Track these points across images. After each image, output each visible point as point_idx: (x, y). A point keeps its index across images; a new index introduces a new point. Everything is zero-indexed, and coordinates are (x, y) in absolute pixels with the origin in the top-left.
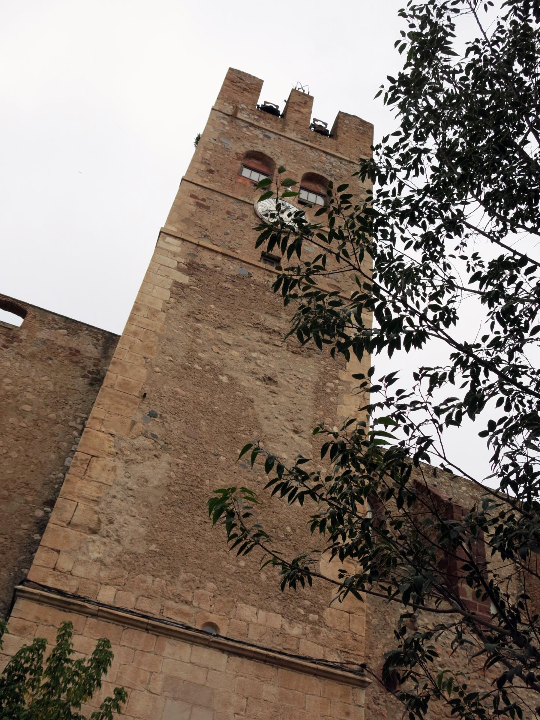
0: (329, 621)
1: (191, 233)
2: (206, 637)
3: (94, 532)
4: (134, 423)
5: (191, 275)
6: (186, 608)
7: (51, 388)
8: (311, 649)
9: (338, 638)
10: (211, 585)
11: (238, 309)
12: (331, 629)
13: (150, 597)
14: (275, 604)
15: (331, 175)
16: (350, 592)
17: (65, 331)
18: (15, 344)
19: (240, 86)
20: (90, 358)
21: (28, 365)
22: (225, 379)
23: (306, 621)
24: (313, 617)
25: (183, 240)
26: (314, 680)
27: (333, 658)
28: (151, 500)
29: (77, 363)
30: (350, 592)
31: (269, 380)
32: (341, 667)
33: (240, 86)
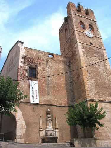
5: (84, 49)
10: (103, 95)
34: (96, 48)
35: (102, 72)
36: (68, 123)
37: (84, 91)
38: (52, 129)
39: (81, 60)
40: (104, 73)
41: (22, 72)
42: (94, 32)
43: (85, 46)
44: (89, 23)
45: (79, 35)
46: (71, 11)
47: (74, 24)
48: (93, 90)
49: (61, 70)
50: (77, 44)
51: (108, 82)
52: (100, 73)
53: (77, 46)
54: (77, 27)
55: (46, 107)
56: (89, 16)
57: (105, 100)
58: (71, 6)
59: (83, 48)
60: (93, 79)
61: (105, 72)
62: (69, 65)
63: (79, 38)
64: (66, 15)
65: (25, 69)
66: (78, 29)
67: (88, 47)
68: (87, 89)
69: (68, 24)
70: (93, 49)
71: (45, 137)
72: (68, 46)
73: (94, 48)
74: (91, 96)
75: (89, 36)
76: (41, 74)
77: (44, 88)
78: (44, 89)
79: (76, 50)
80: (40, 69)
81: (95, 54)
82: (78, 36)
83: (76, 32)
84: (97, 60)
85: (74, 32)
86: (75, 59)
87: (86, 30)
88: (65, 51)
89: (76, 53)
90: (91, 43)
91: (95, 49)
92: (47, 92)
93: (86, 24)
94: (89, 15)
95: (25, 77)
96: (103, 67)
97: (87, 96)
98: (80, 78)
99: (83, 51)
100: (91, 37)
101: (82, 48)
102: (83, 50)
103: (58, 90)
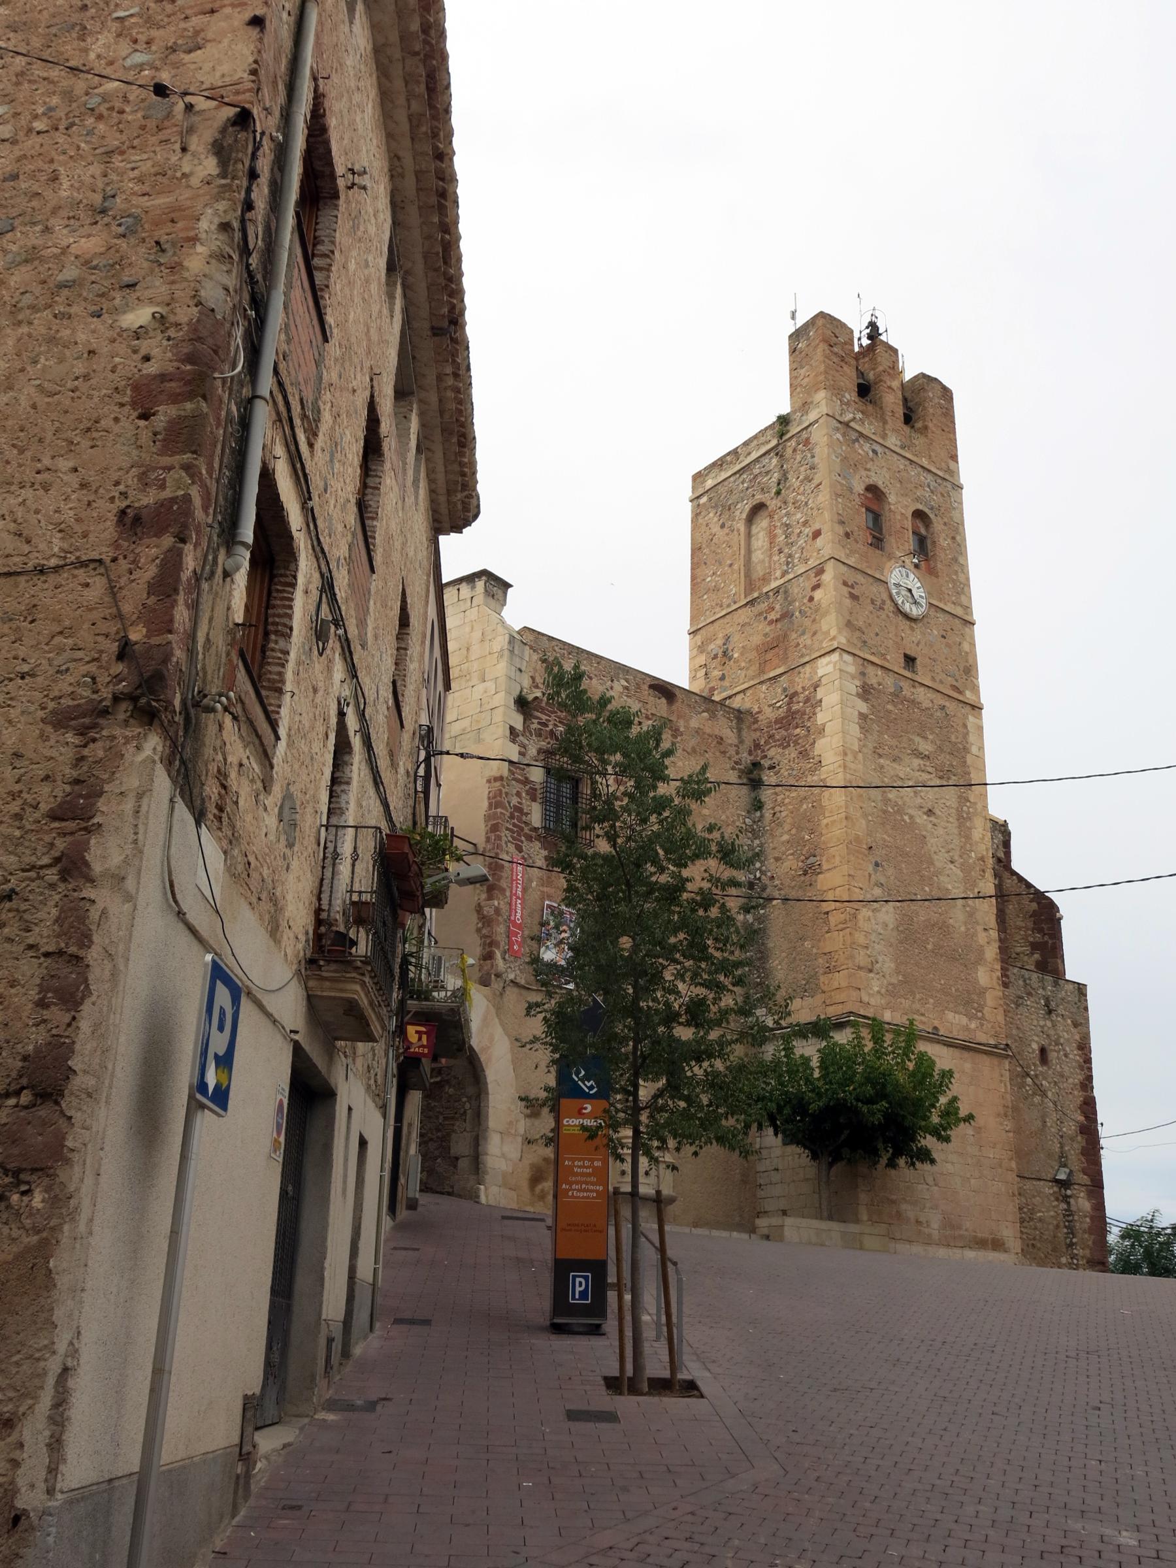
0: (987, 1016)
3: (871, 971)
4: (870, 875)
5: (866, 700)
6: (923, 1018)
8: (982, 1037)
10: (931, 1001)
11: (9, 706)
14: (961, 1008)
17: (705, 714)
19: (511, 586)
20: (731, 745)
22: (906, 818)
24: (979, 1014)
25: (854, 655)
26: (985, 1057)
27: (992, 1042)
28: (892, 940)
31: (930, 812)
32: (995, 1047)
33: (511, 586)
34: (931, 695)
35: (940, 860)
36: (55, 1285)
40: (952, 862)
41: (515, 801)
42: (932, 572)
43: (873, 681)
45: (854, 597)
48: (887, 964)
51: (965, 923)
52: (931, 862)
56: (920, 441)
57: (935, 1028)
61: (956, 858)
64: (785, 409)
65: (526, 781)
66: (852, 552)
67: (889, 682)
70: (914, 703)
71: (54, 1366)
72: (757, 639)
73: (922, 695)
74: (873, 1001)
79: (820, 693)
81: (917, 739)
86: (804, 754)
87: (890, 557)
90: (910, 660)
93: (899, 506)
96: (953, 828)
99: (860, 714)
102: (863, 707)
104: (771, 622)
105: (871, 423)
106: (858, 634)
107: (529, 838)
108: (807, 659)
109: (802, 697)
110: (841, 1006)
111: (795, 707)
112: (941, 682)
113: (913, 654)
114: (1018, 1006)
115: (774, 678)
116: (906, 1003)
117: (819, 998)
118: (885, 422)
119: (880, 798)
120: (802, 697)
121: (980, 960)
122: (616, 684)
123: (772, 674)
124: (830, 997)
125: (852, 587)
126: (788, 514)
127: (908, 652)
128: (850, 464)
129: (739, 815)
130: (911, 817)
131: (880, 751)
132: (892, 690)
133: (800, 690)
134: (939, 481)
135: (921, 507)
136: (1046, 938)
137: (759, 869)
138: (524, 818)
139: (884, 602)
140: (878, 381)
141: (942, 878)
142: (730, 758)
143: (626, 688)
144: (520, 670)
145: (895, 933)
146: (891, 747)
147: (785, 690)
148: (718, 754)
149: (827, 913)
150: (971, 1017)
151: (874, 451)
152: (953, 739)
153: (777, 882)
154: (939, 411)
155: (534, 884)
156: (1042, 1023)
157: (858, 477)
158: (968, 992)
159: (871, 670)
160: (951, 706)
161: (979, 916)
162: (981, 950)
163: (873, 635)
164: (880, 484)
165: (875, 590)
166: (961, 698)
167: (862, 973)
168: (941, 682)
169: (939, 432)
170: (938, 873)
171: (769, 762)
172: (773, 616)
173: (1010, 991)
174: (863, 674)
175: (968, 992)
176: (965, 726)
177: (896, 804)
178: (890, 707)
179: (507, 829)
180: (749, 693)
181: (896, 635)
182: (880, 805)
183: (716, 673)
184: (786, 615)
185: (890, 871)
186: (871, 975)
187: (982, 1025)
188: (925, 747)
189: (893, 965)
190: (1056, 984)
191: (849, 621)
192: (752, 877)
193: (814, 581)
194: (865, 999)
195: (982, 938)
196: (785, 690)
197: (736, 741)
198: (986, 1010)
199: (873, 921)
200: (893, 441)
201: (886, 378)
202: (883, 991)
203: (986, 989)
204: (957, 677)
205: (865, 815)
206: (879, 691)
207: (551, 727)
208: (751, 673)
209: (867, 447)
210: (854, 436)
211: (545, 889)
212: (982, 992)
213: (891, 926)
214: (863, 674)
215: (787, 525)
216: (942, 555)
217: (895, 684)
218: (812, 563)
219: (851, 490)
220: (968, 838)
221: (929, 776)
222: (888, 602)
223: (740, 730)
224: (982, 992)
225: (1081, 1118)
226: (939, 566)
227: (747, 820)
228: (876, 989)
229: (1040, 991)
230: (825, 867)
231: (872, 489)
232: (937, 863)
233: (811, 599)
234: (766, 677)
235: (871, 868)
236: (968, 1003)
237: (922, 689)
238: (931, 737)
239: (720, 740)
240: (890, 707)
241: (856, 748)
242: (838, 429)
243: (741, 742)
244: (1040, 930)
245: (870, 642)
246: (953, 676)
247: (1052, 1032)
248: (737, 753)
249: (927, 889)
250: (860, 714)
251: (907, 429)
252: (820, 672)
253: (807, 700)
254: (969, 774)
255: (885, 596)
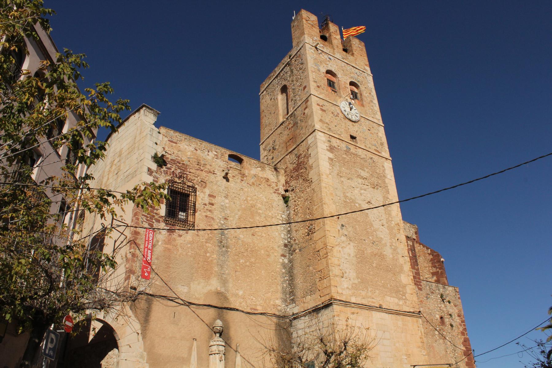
1: (325, 128)
2: (380, 308)
4: (339, 231)
5: (332, 152)
6: (373, 300)
7: (265, 200)
9: (411, 303)
10: (377, 291)
12: (409, 301)
13: (364, 298)
14: (394, 295)
15: (359, 82)
16: (102, 325)
17: (260, 169)
18: (245, 178)
20: (273, 182)
21: (253, 189)
22: (357, 205)
23: (402, 299)
27: (412, 311)
29: (270, 185)
30: (102, 325)
31: (274, 149)
32: (413, 313)
34: (365, 152)
37: (324, 275)
38: (223, 344)
39: (323, 185)
42: (363, 105)
43: (336, 145)
44: (352, 77)
46: (306, 36)
47: (312, 76)
48: (352, 274)
49: (259, 205)
50: (316, 138)
52: (372, 225)
53: (316, 144)
54: (318, 87)
55: (212, 311)
56: (351, 58)
58: (304, 20)
59: (331, 149)
60: (352, 244)
61: (385, 223)
62: (283, 193)
63: (321, 120)
66: (321, 93)
67: (343, 146)
68: (335, 271)
69: (292, 71)
72: (285, 137)
74: (344, 292)
75: (350, 117)
76: (205, 214)
77: (208, 255)
78: (209, 258)
80: (201, 198)
81: (360, 171)
82: (320, 112)
83: (313, 99)
84: (365, 187)
85: (307, 101)
87: (340, 97)
88: (274, 149)
89: (311, 161)
90: (353, 138)
91: (363, 156)
92: (216, 269)
94: (353, 54)
95: (156, 217)
97: (333, 289)
98: (316, 236)
99: (329, 158)
100: (354, 119)
101: (327, 150)
102: (331, 155)
103: (248, 264)
104: (289, 129)
105: (327, 49)
106: (326, 125)
107: (158, 221)
108: (304, 138)
109: (303, 156)
110: (327, 296)
111: (300, 160)
112: (370, 148)
113: (354, 135)
114: (427, 298)
115: (292, 151)
116: (363, 293)
117: (318, 293)
118: (334, 49)
119: (342, 195)
120: (303, 156)
121: (401, 271)
122: (210, 153)
123: (290, 150)
124: (322, 292)
125: (322, 106)
126: (294, 85)
127: (352, 135)
128: (317, 62)
129: (278, 214)
130: (359, 204)
131: (341, 175)
132: (345, 149)
133: (301, 152)
134: (361, 72)
135: (353, 81)
136: (438, 270)
137: (290, 237)
138: (155, 211)
139: (338, 114)
140: (330, 35)
141: (378, 233)
142: (273, 188)
143: (216, 155)
144: (156, 144)
145: (355, 259)
146: (346, 173)
147: (296, 155)
148: (266, 186)
149: (318, 251)
150: (400, 299)
151: (329, 58)
152: (378, 171)
153: (297, 241)
154: (359, 49)
155: (160, 243)
156: (440, 306)
157: (322, 66)
158: (397, 286)
159: (333, 140)
160: (375, 158)
161: (399, 250)
162: (401, 266)
163: (334, 126)
164: (333, 70)
165: (333, 108)
166: (379, 154)
167: (337, 278)
168: (370, 148)
169: (359, 56)
170: (375, 231)
171: (292, 188)
172: (290, 126)
173: (424, 292)
174: (330, 141)
175: (397, 286)
176: (383, 167)
177: (351, 199)
178: (344, 156)
179: (143, 215)
180: (282, 161)
181: (345, 127)
182: (343, 198)
183: (270, 157)
184: (295, 124)
185: (350, 229)
186: (343, 279)
187: (406, 303)
188: (364, 174)
189: (355, 274)
190: (444, 288)
191: (321, 119)
192: (286, 241)
193: (305, 106)
194: (340, 291)
195: (401, 261)
196: (296, 155)
197: (276, 181)
198: (407, 295)
199: (342, 252)
200: (338, 56)
201: (332, 34)
202: (350, 287)
203: (406, 285)
204: (377, 146)
205: (335, 203)
206: (338, 149)
207: (173, 170)
208: (282, 152)
209: (326, 56)
210: (320, 52)
211: (166, 246)
212: (404, 286)
213: (352, 255)
214: (330, 141)
215: (294, 89)
216: (365, 99)
217: (347, 147)
218: (304, 99)
219: (319, 70)
220: (390, 215)
221: (368, 187)
222: (341, 114)
223: (277, 176)
224: (404, 286)
225: (464, 348)
226: (364, 103)
227: (283, 216)
228: (346, 286)
229: (437, 291)
230: (316, 229)
231: (329, 72)
232: (375, 226)
233: (304, 113)
234: (288, 152)
235: (339, 228)
236: (397, 292)
237: (361, 150)
238: (367, 170)
239: (267, 180)
240: (344, 156)
241: (328, 172)
242: (311, 48)
243: (279, 181)
244: (435, 267)
245: (332, 129)
246: (375, 146)
247: (445, 309)
248: (277, 186)
249: (371, 238)
250: (329, 158)
251: (344, 53)
252: (309, 142)
253: (305, 156)
254: (387, 187)
255: (339, 112)
